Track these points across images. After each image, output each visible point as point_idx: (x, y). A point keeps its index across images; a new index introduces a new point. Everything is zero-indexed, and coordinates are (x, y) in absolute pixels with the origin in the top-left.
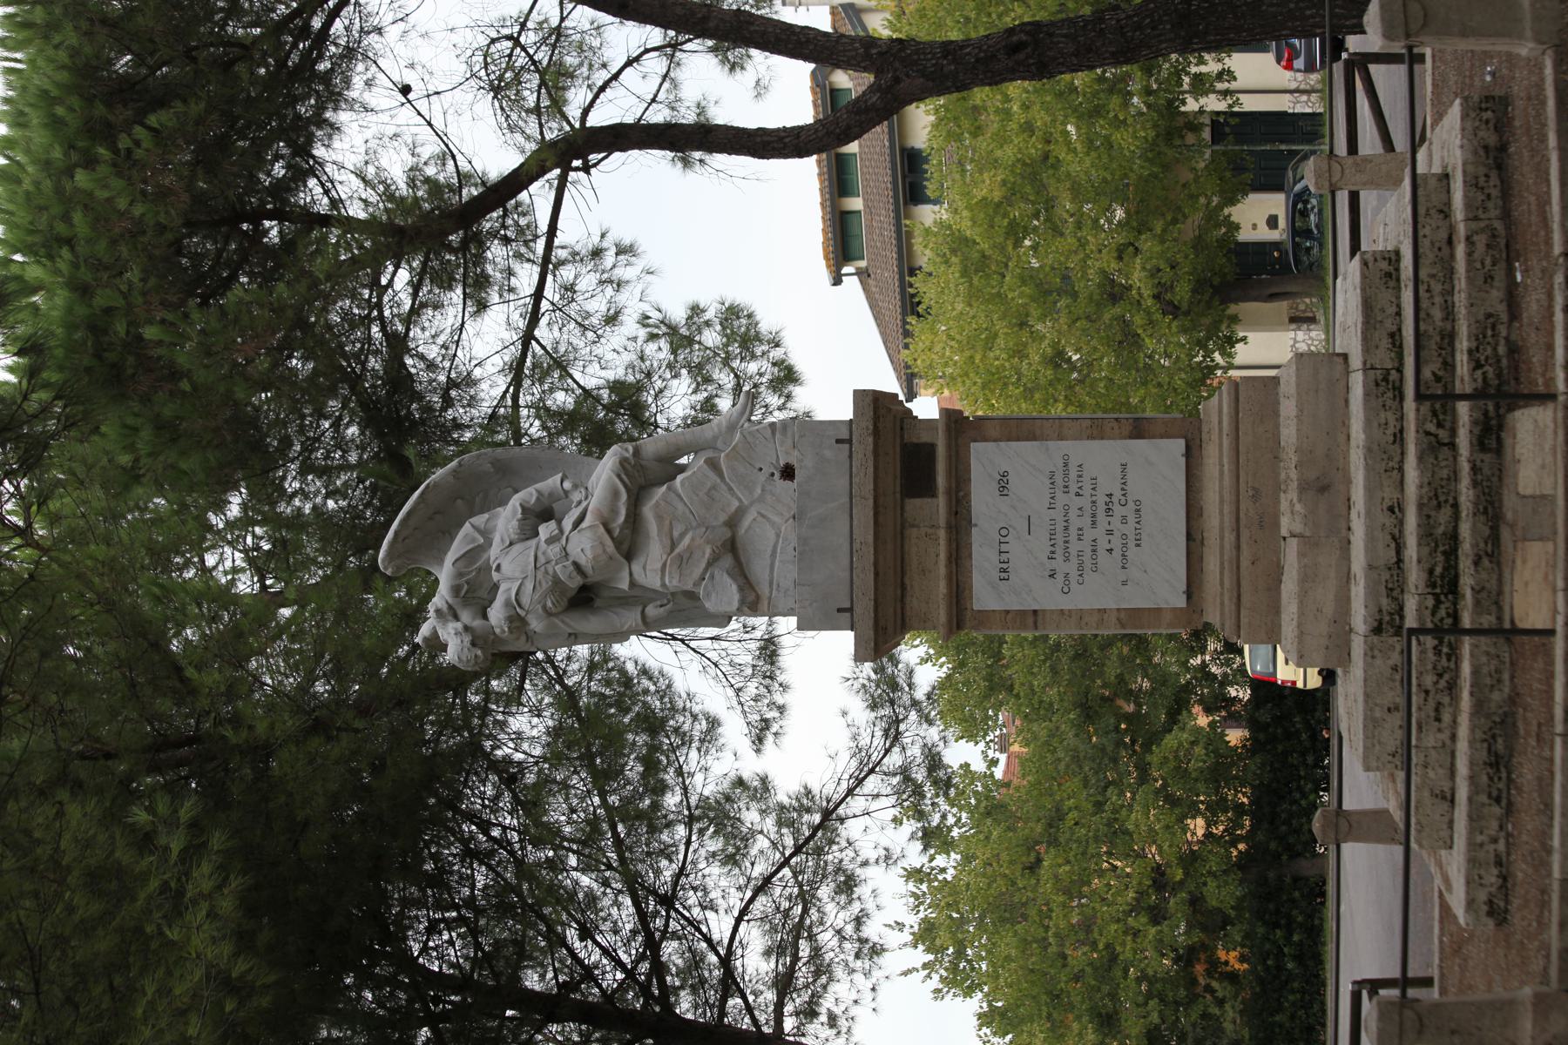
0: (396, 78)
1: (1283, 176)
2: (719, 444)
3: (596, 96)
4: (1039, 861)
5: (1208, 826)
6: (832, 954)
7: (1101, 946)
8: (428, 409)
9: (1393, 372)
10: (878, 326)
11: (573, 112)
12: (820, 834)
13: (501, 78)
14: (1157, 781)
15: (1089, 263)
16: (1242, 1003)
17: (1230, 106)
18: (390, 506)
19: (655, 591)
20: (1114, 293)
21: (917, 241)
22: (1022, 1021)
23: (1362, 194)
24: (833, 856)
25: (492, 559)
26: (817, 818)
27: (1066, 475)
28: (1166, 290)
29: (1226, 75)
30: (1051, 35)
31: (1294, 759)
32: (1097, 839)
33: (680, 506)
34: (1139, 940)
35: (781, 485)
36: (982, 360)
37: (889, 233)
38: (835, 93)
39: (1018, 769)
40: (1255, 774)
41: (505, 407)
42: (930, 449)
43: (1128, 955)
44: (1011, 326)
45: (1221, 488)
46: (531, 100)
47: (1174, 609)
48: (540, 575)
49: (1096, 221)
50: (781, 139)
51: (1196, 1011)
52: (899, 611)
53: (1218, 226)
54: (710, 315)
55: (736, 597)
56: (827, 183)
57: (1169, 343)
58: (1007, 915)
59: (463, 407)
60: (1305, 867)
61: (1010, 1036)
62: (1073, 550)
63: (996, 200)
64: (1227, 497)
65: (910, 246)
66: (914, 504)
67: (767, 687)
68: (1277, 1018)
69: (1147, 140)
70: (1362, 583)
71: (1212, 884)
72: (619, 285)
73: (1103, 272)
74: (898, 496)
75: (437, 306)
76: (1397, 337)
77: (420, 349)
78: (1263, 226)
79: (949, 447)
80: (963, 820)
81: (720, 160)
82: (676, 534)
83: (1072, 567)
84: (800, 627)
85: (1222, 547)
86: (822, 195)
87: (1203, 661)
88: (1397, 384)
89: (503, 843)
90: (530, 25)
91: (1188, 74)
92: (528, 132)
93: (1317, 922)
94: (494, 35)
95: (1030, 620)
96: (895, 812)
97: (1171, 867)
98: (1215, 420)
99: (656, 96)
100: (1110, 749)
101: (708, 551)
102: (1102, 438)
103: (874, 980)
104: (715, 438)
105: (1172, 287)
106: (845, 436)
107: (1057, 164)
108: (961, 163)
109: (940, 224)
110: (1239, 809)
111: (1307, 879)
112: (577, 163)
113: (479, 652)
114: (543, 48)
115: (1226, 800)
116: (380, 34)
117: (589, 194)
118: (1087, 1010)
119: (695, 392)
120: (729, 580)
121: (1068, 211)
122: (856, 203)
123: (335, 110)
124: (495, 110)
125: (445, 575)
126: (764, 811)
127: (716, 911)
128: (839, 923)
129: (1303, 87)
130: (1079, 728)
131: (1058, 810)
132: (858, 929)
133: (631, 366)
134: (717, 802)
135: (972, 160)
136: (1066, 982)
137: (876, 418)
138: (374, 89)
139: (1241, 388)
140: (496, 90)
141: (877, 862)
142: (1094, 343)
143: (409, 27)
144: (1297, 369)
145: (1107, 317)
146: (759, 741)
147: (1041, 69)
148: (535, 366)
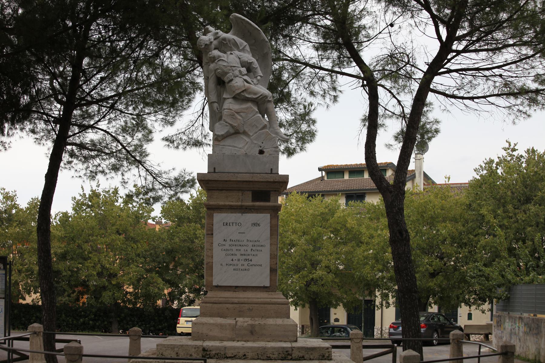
0: (396, 22)
2: (271, 129)
3: (388, 90)
4: (120, 234)
5: (130, 293)
6: (92, 162)
7: (90, 255)
8: (283, 29)
9: (291, 357)
10: (304, 183)
11: (383, 82)
12: (133, 159)
16: (68, 304)
17: (377, 306)
20: (314, 265)
21: (334, 198)
22: (64, 227)
23: (349, 350)
27: (258, 246)
28: (314, 283)
29: (388, 305)
30: (405, 245)
31: (152, 323)
32: (127, 254)
33: (251, 116)
34: (92, 268)
36: (292, 219)
37: (336, 188)
38: (385, 170)
40: (148, 309)
41: (283, 56)
42: (268, 200)
45: (253, 298)
47: (212, 281)
48: (229, 68)
49: (339, 259)
50: (372, 152)
52: (214, 188)
53: (336, 301)
54: (312, 127)
57: (296, 283)
58: (101, 223)
59: (283, 42)
60: (115, 326)
61: (59, 223)
62: (233, 248)
63: (347, 225)
65: (332, 195)
66: (250, 194)
67: (185, 143)
68: (63, 315)
70: (220, 345)
71: (110, 294)
72: (323, 96)
73: (321, 261)
74: (253, 189)
76: (302, 359)
77: (303, 27)
79: (268, 207)
80: (134, 209)
81: (365, 131)
82: (242, 114)
83: (227, 247)
84: (209, 155)
85: (233, 298)
86: (350, 165)
87: (186, 292)
88: (287, 358)
89: (133, 51)
90: (413, 68)
92: (377, 67)
94: (410, 56)
95: (210, 233)
96: (139, 185)
99: (387, 110)
101: (236, 125)
102: (270, 258)
103: (83, 177)
104: (273, 128)
108: (360, 213)
109: (339, 206)
110: (135, 304)
112: (365, 82)
113: (203, 47)
116: (411, 17)
117: (354, 86)
119: (287, 121)
120: (225, 131)
122: (346, 177)
124: (384, 55)
126: (140, 140)
127: (108, 124)
128: (102, 165)
129: (383, 332)
131: (137, 241)
132: (100, 172)
133: (296, 99)
135: (361, 217)
137: (279, 182)
138: (392, 15)
139: (286, 306)
140: (392, 56)
141: (123, 179)
143: (413, 27)
144: (292, 325)
146: (166, 139)
147: (393, 241)
148: (297, 67)
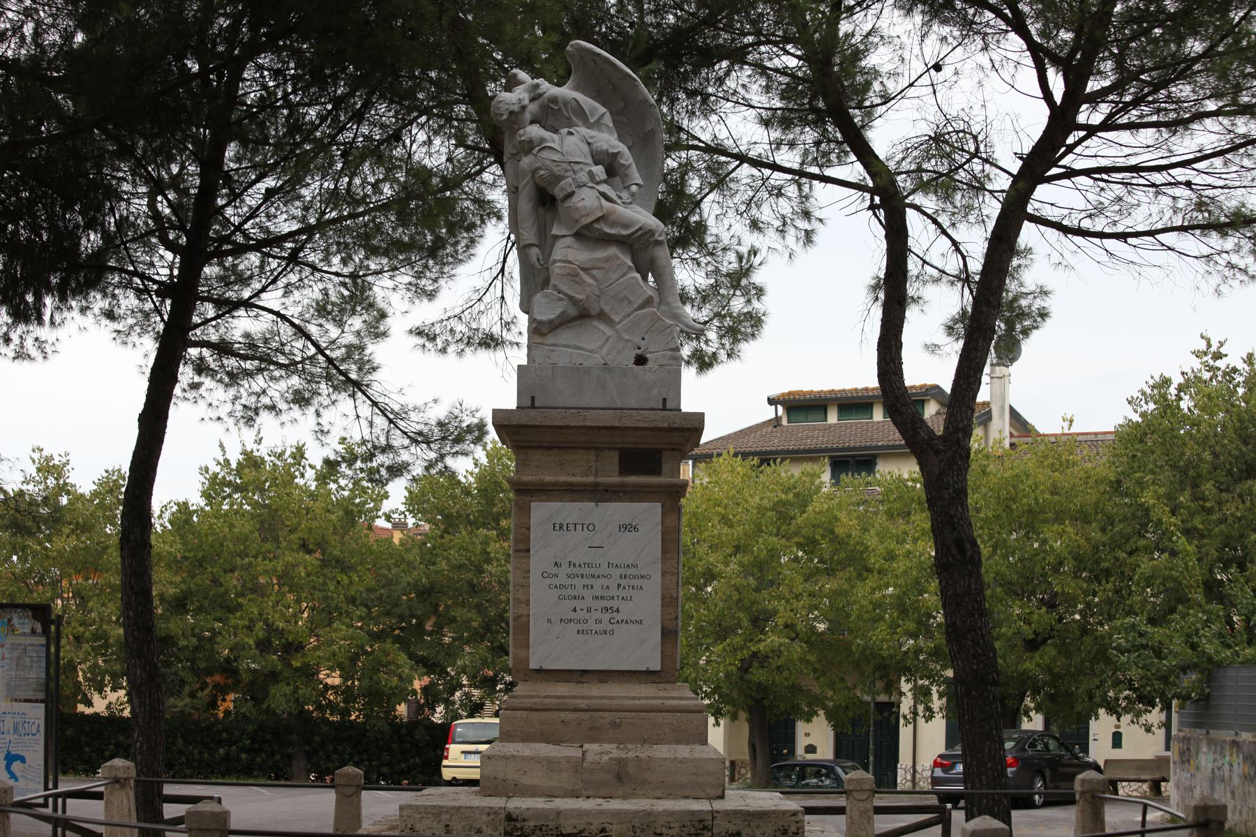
0: (947, 60)
1: (848, 758)
2: (663, 307)
3: (929, 216)
4: (310, 552)
7: (240, 600)
8: (685, 77)
10: (735, 433)
11: (918, 199)
12: (342, 378)
13: (946, 142)
14: (371, 647)
15: (783, 601)
16: (190, 714)
17: (905, 717)
18: (604, 42)
19: (550, 255)
20: (759, 621)
21: (808, 467)
22: (182, 537)
24: (324, 388)
25: (577, 129)
26: (353, 376)
27: (634, 577)
29: (930, 715)
30: (970, 574)
31: (386, 757)
32: (326, 598)
33: (616, 276)
34: (244, 630)
35: (631, 354)
37: (809, 444)
39: (383, 537)
40: (375, 726)
41: (687, 139)
42: (657, 472)
43: (233, 622)
44: (739, 539)
45: (623, 698)
46: (925, 166)
48: (565, 166)
49: (816, 607)
50: (893, 360)
51: (187, 676)
52: (532, 444)
53: (810, 705)
55: (544, 318)
56: (839, 395)
57: (719, 663)
58: (266, 526)
59: (687, 106)
60: (299, 764)
61: (170, 527)
62: (576, 581)
64: (615, 702)
66: (614, 457)
67: (461, 339)
69: (880, 650)
70: (546, 806)
71: (288, 690)
73: (775, 612)
74: (621, 446)
75: (767, 89)
78: (807, 741)
79: (659, 486)
81: (877, 313)
82: (595, 272)
85: (575, 697)
86: (840, 391)
90: (987, 167)
91: (931, 684)
92: (904, 163)
93: (255, 773)
94: (980, 138)
95: (522, 547)
97: (302, 657)
98: (675, 694)
99: (928, 264)
100: (397, 610)
101: (581, 297)
103: (226, 419)
104: (668, 304)
105: (763, 667)
106: (669, 405)
107: (860, 577)
108: (864, 502)
110: (345, 713)
111: (290, 766)
112: (877, 200)
113: (505, 117)
114: (969, 176)
115: (355, 701)
116: (982, 49)
117: (852, 209)
118: (190, 587)
119: (698, 292)
120: (557, 313)
121: (823, 586)
122: (833, 418)
123: (923, 12)
125: (566, 91)
127: (283, 296)
128: (270, 392)
129: (918, 776)
130: (415, 586)
131: (350, 568)
134: (367, 297)
135: (867, 511)
136: (212, 573)
137: (681, 430)
138: (939, 42)
141: (319, 424)
142: (721, 604)
144: (713, 759)
145: (741, 615)
146: (419, 332)
147: (942, 566)
148: (719, 163)
